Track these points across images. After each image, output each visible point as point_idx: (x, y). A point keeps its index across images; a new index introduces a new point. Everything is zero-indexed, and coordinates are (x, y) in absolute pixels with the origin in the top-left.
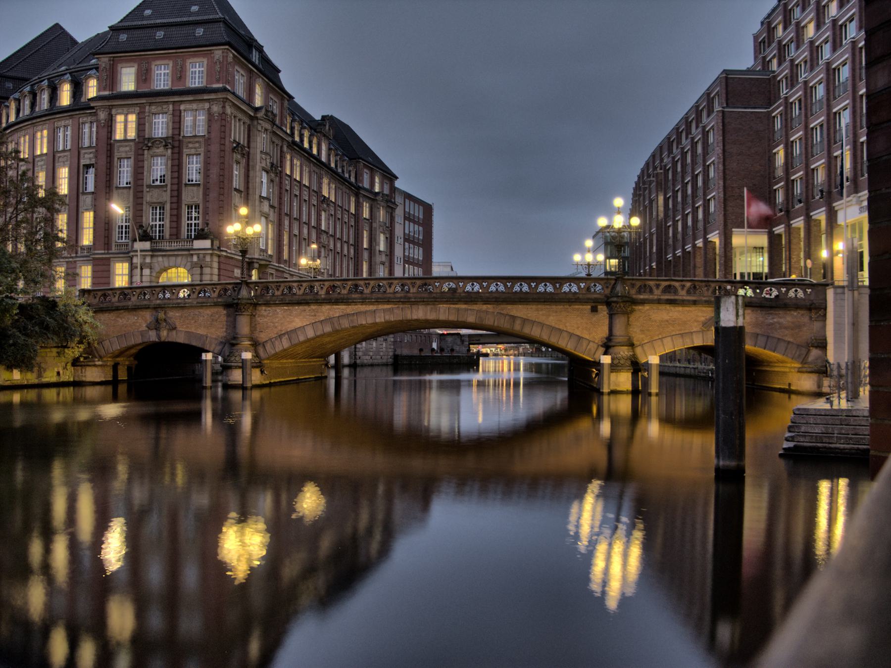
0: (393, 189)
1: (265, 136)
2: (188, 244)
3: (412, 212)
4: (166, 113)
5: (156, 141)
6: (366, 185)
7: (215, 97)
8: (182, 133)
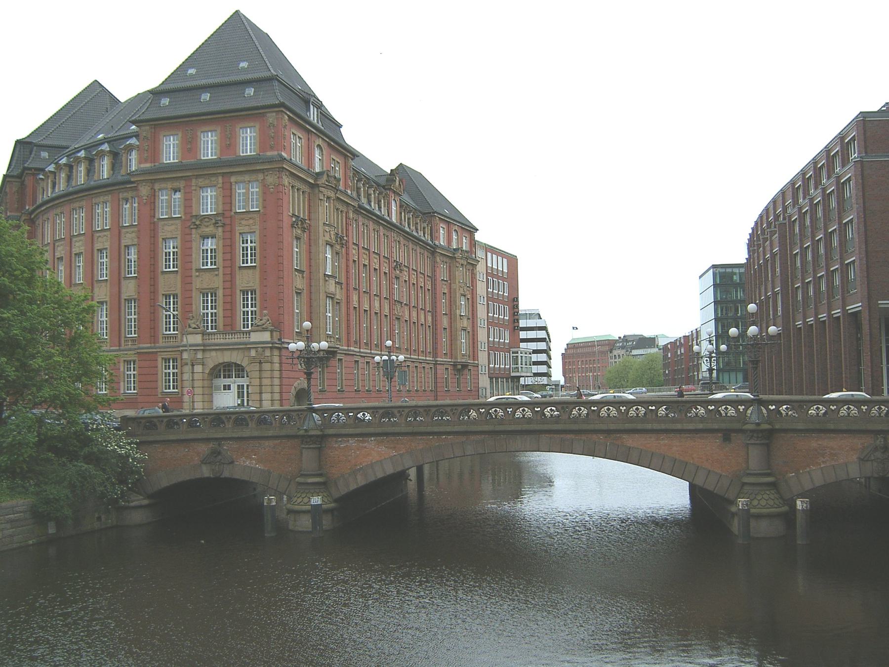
0: (473, 243)
1: (327, 204)
2: (245, 336)
3: (495, 267)
4: (215, 186)
5: (205, 218)
6: (442, 242)
7: (269, 167)
8: (233, 208)
